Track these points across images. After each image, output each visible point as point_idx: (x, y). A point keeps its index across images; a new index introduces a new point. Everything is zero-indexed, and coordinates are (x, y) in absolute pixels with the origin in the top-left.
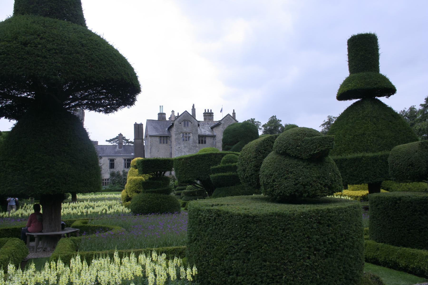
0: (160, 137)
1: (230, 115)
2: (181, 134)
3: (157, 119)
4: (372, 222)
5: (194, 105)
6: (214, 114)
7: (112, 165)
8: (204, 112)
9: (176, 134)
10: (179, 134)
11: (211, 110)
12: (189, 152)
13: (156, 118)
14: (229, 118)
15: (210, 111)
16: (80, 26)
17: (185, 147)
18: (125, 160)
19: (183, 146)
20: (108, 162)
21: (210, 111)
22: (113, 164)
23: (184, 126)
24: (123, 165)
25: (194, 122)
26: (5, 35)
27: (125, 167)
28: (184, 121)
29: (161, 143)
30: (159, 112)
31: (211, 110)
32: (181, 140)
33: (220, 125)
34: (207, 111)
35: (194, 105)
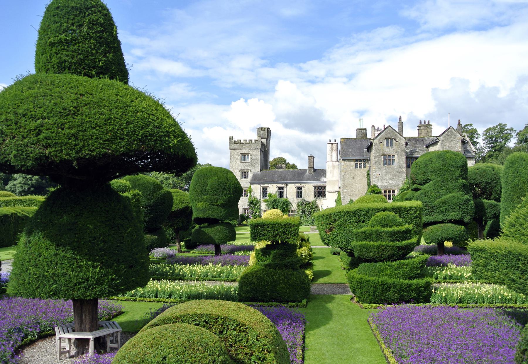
0: (356, 160)
1: (453, 128)
2: (383, 156)
3: (355, 137)
4: (133, 94)
5: (459, 120)
6: (432, 127)
7: (299, 194)
8: (419, 124)
9: (376, 157)
10: (380, 156)
11: (429, 122)
12: (392, 179)
13: (354, 135)
14: (451, 132)
15: (427, 123)
16: (118, 83)
17: (387, 173)
18: (315, 187)
19: (384, 171)
20: (295, 190)
21: (427, 123)
22: (301, 192)
23: (387, 145)
24: (313, 193)
25: (400, 139)
26: (90, 108)
27: (315, 196)
28: (387, 139)
29: (356, 167)
30: (359, 127)
31: (429, 122)
32: (382, 164)
33: (438, 142)
34: (423, 123)
35: (459, 120)
